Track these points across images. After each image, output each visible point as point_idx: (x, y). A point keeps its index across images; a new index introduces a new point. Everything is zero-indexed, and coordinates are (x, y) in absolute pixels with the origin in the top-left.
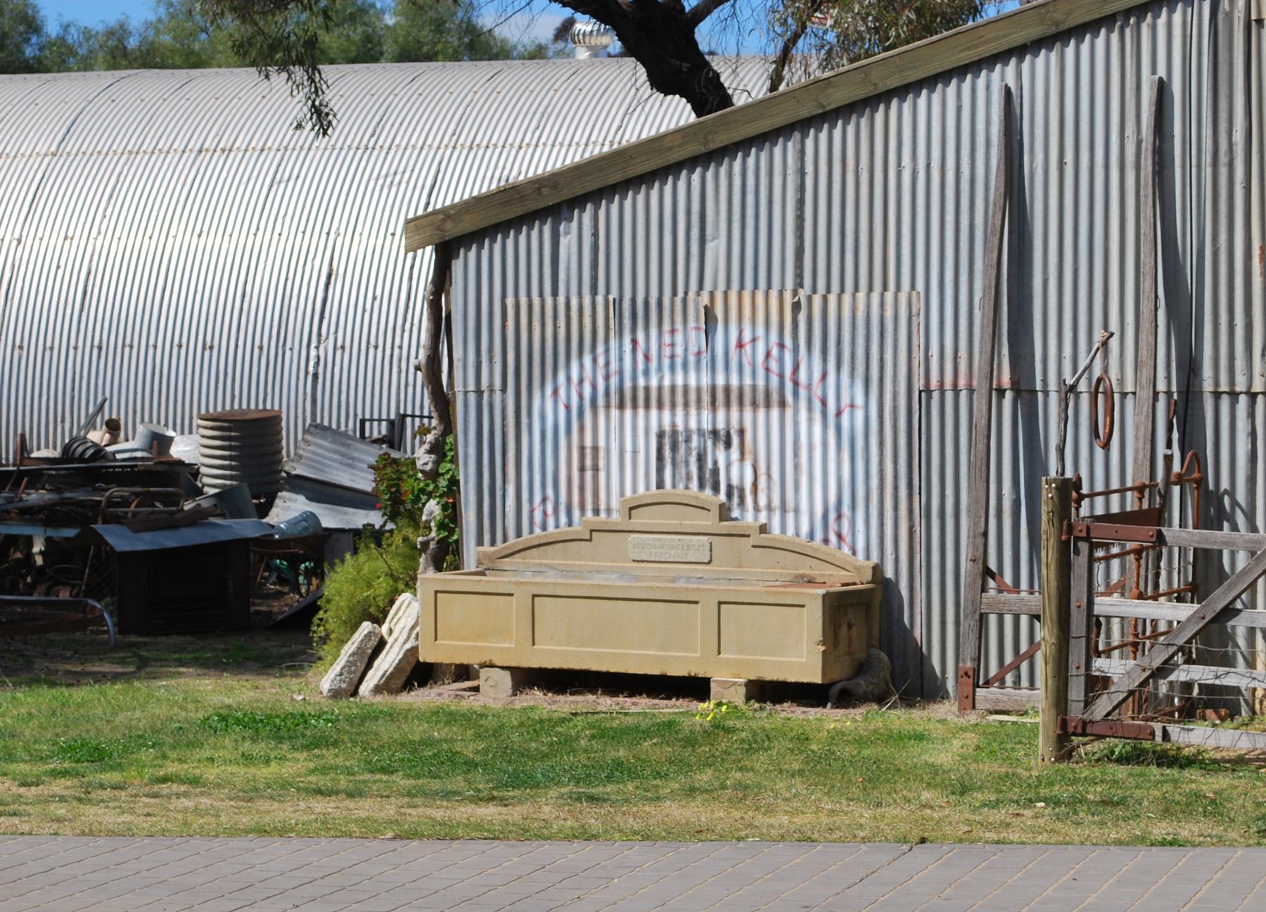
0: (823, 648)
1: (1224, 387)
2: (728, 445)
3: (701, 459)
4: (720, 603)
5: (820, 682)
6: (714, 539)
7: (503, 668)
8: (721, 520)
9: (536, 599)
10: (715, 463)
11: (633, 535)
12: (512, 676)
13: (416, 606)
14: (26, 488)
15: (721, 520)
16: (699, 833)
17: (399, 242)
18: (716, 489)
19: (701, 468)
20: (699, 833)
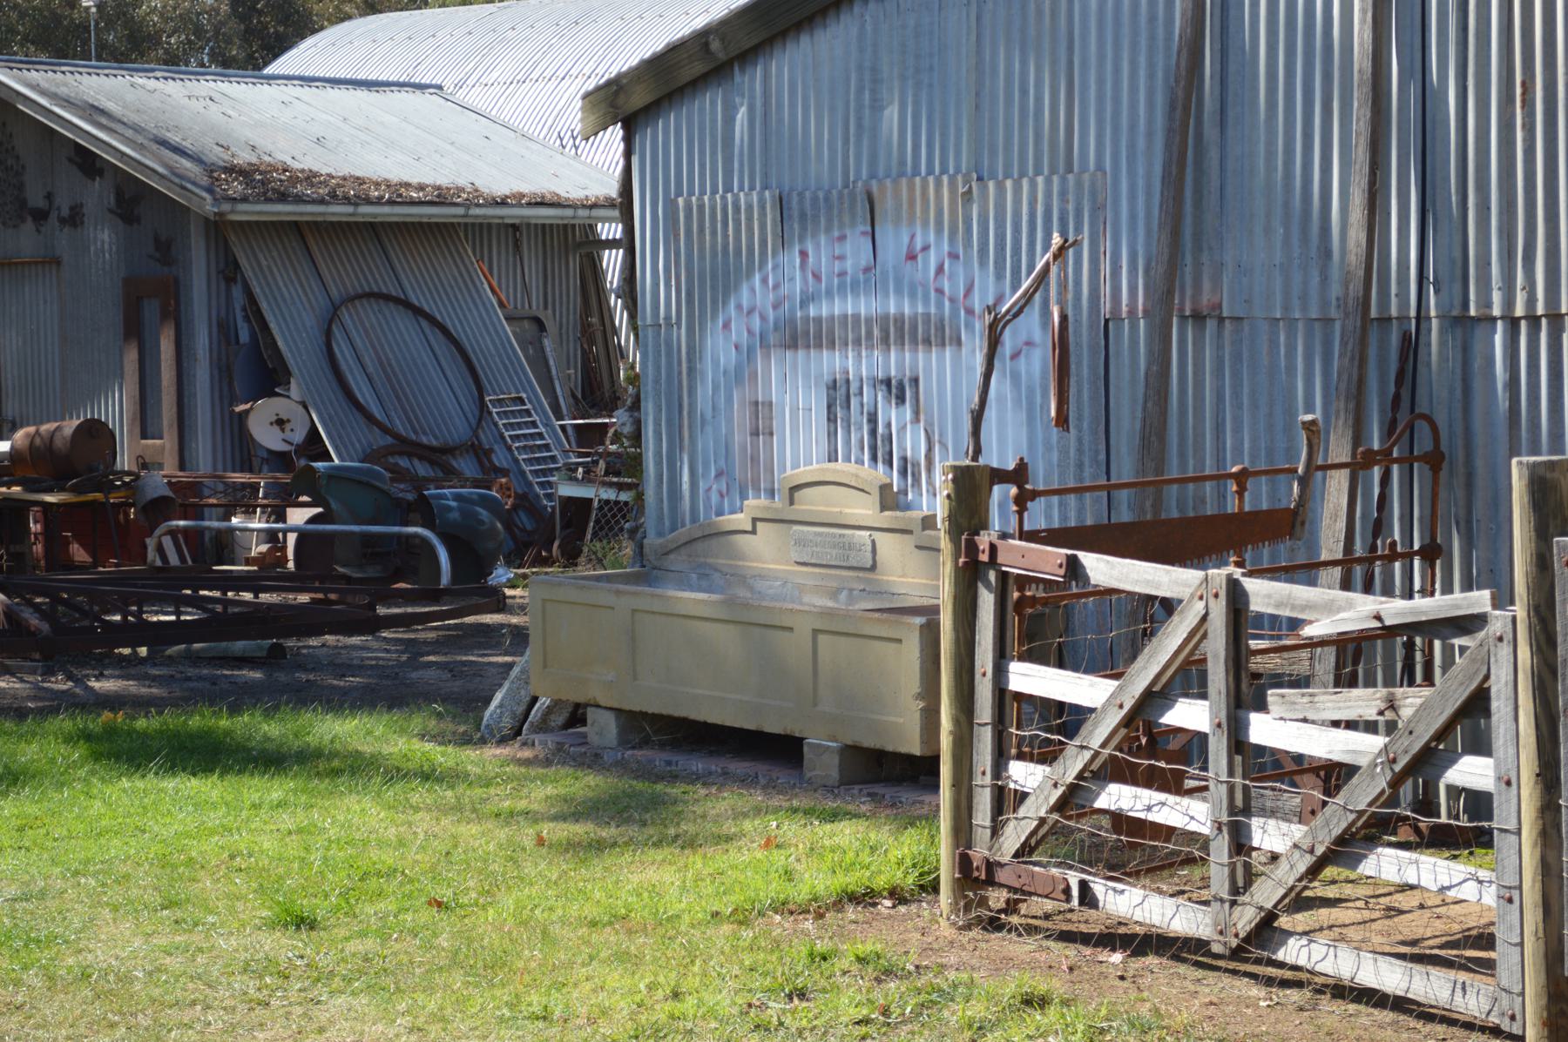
0: (922, 705)
1: (1519, 311)
2: (901, 399)
3: (873, 419)
4: (816, 632)
5: (918, 753)
6: (877, 535)
7: (611, 709)
8: (882, 510)
9: (821, 637)
10: (889, 425)
11: (796, 528)
12: (617, 718)
13: (76, 546)
14: (108, 487)
15: (882, 510)
16: (428, 776)
17: (574, 117)
18: (889, 463)
19: (873, 432)
20: (428, 776)
